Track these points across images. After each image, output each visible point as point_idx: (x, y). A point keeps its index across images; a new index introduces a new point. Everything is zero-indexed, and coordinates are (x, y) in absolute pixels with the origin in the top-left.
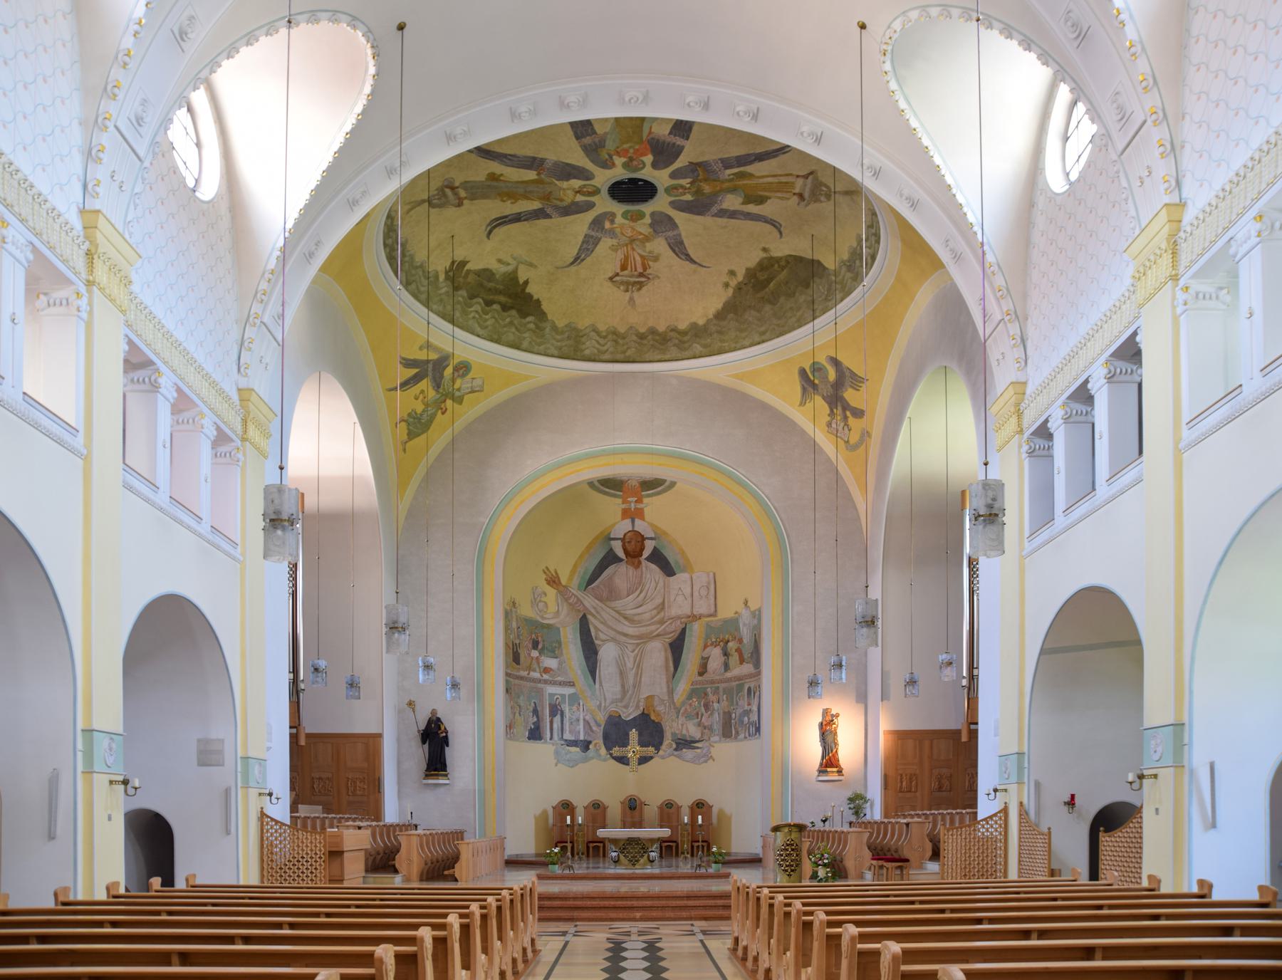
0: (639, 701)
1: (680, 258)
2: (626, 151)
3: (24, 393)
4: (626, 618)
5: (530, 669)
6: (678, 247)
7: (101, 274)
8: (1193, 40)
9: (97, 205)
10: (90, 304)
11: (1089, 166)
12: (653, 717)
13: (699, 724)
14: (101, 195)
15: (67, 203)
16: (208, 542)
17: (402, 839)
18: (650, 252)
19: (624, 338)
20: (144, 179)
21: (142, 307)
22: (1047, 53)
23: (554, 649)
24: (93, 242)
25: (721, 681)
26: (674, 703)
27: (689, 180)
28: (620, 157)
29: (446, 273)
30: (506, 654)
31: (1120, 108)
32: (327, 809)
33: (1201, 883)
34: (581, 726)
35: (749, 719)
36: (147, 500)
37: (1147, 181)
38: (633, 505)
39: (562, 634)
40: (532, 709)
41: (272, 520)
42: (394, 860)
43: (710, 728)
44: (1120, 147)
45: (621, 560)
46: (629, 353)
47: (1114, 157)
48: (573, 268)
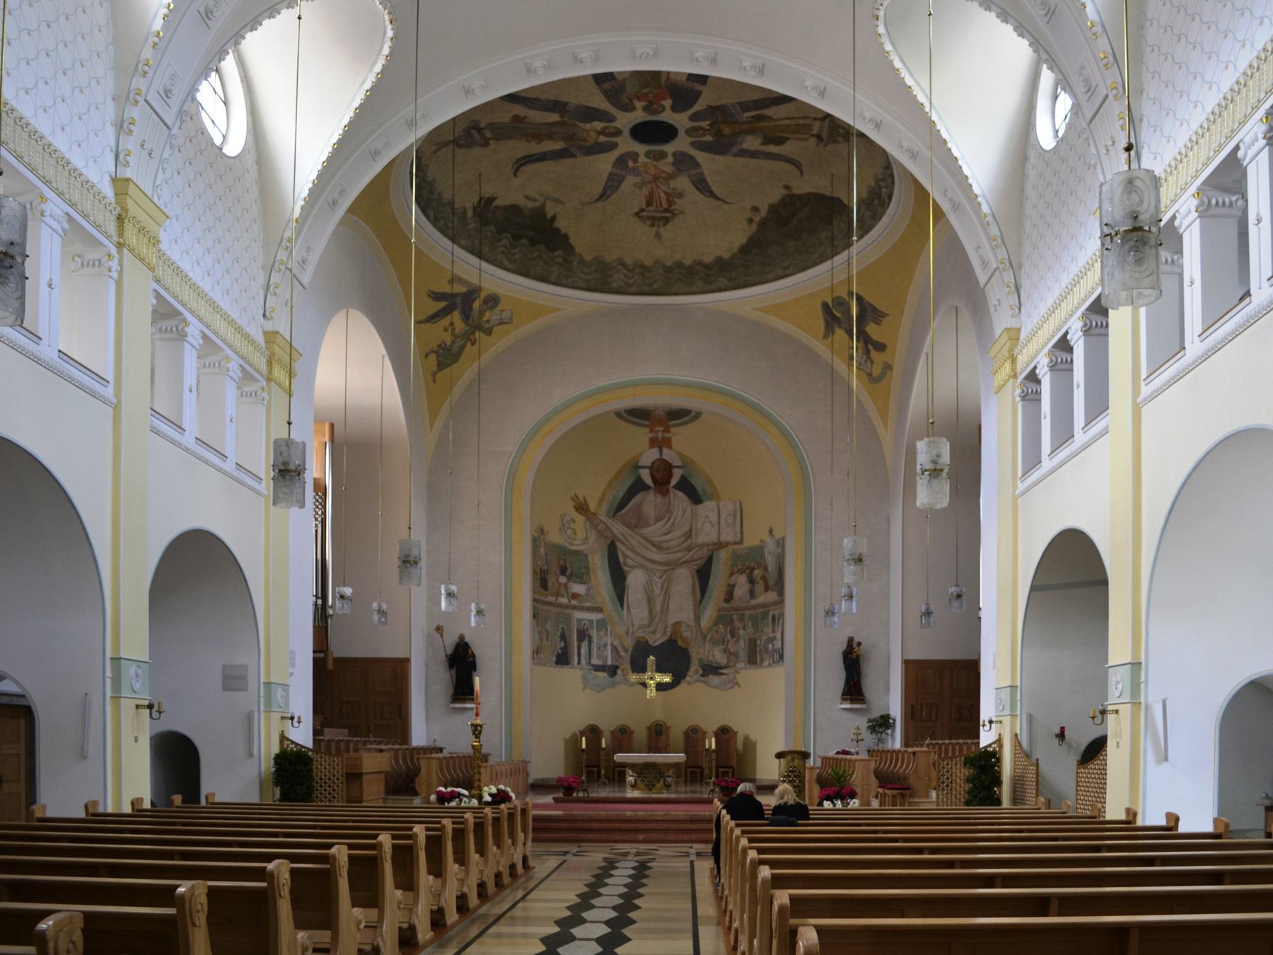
0: (666, 628)
1: (704, 194)
2: (646, 95)
3: (60, 351)
4: (654, 545)
5: (557, 594)
6: (702, 185)
7: (131, 236)
8: (1149, 23)
9: (128, 173)
10: (121, 264)
11: (1070, 127)
12: (680, 643)
13: (725, 651)
14: (131, 164)
15: (100, 175)
16: (233, 478)
17: (423, 764)
18: (674, 189)
19: (651, 272)
20: (172, 146)
21: (169, 263)
22: (1022, 25)
23: (582, 575)
24: (125, 209)
25: (746, 608)
26: (701, 630)
27: (708, 123)
28: (640, 100)
29: (474, 209)
30: (534, 580)
31: (1087, 81)
32: (354, 731)
33: (1169, 815)
34: (609, 652)
35: (773, 646)
36: (173, 442)
37: (1112, 149)
38: (660, 434)
39: (590, 560)
40: (559, 634)
41: (280, 471)
42: (414, 782)
43: (736, 655)
44: (1089, 117)
45: (648, 488)
46: (655, 286)
47: (1085, 126)
48: (600, 204)
